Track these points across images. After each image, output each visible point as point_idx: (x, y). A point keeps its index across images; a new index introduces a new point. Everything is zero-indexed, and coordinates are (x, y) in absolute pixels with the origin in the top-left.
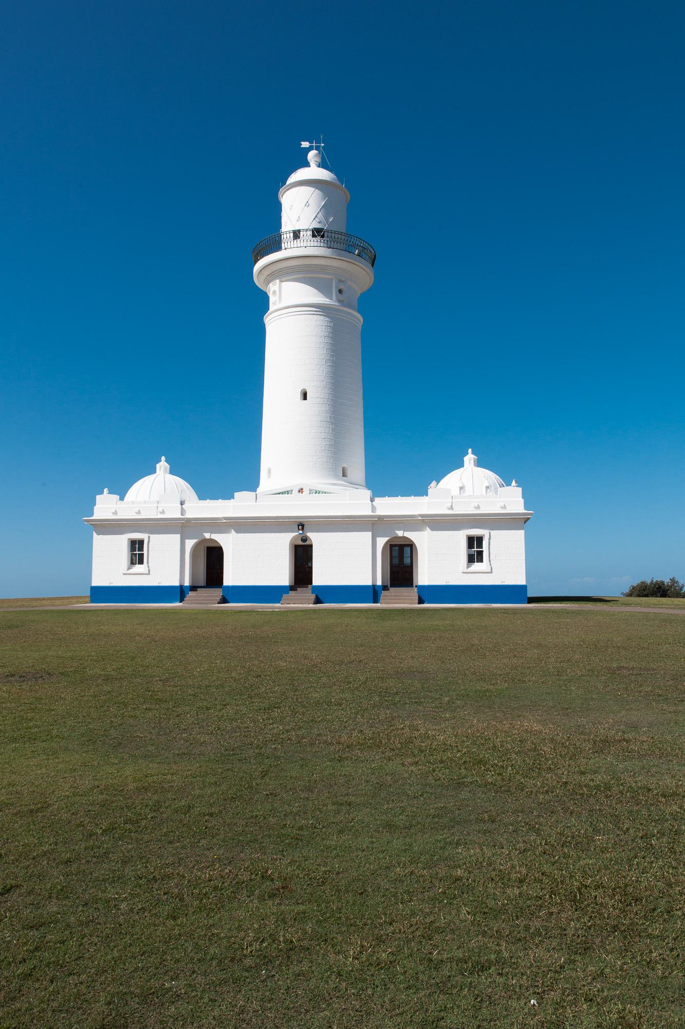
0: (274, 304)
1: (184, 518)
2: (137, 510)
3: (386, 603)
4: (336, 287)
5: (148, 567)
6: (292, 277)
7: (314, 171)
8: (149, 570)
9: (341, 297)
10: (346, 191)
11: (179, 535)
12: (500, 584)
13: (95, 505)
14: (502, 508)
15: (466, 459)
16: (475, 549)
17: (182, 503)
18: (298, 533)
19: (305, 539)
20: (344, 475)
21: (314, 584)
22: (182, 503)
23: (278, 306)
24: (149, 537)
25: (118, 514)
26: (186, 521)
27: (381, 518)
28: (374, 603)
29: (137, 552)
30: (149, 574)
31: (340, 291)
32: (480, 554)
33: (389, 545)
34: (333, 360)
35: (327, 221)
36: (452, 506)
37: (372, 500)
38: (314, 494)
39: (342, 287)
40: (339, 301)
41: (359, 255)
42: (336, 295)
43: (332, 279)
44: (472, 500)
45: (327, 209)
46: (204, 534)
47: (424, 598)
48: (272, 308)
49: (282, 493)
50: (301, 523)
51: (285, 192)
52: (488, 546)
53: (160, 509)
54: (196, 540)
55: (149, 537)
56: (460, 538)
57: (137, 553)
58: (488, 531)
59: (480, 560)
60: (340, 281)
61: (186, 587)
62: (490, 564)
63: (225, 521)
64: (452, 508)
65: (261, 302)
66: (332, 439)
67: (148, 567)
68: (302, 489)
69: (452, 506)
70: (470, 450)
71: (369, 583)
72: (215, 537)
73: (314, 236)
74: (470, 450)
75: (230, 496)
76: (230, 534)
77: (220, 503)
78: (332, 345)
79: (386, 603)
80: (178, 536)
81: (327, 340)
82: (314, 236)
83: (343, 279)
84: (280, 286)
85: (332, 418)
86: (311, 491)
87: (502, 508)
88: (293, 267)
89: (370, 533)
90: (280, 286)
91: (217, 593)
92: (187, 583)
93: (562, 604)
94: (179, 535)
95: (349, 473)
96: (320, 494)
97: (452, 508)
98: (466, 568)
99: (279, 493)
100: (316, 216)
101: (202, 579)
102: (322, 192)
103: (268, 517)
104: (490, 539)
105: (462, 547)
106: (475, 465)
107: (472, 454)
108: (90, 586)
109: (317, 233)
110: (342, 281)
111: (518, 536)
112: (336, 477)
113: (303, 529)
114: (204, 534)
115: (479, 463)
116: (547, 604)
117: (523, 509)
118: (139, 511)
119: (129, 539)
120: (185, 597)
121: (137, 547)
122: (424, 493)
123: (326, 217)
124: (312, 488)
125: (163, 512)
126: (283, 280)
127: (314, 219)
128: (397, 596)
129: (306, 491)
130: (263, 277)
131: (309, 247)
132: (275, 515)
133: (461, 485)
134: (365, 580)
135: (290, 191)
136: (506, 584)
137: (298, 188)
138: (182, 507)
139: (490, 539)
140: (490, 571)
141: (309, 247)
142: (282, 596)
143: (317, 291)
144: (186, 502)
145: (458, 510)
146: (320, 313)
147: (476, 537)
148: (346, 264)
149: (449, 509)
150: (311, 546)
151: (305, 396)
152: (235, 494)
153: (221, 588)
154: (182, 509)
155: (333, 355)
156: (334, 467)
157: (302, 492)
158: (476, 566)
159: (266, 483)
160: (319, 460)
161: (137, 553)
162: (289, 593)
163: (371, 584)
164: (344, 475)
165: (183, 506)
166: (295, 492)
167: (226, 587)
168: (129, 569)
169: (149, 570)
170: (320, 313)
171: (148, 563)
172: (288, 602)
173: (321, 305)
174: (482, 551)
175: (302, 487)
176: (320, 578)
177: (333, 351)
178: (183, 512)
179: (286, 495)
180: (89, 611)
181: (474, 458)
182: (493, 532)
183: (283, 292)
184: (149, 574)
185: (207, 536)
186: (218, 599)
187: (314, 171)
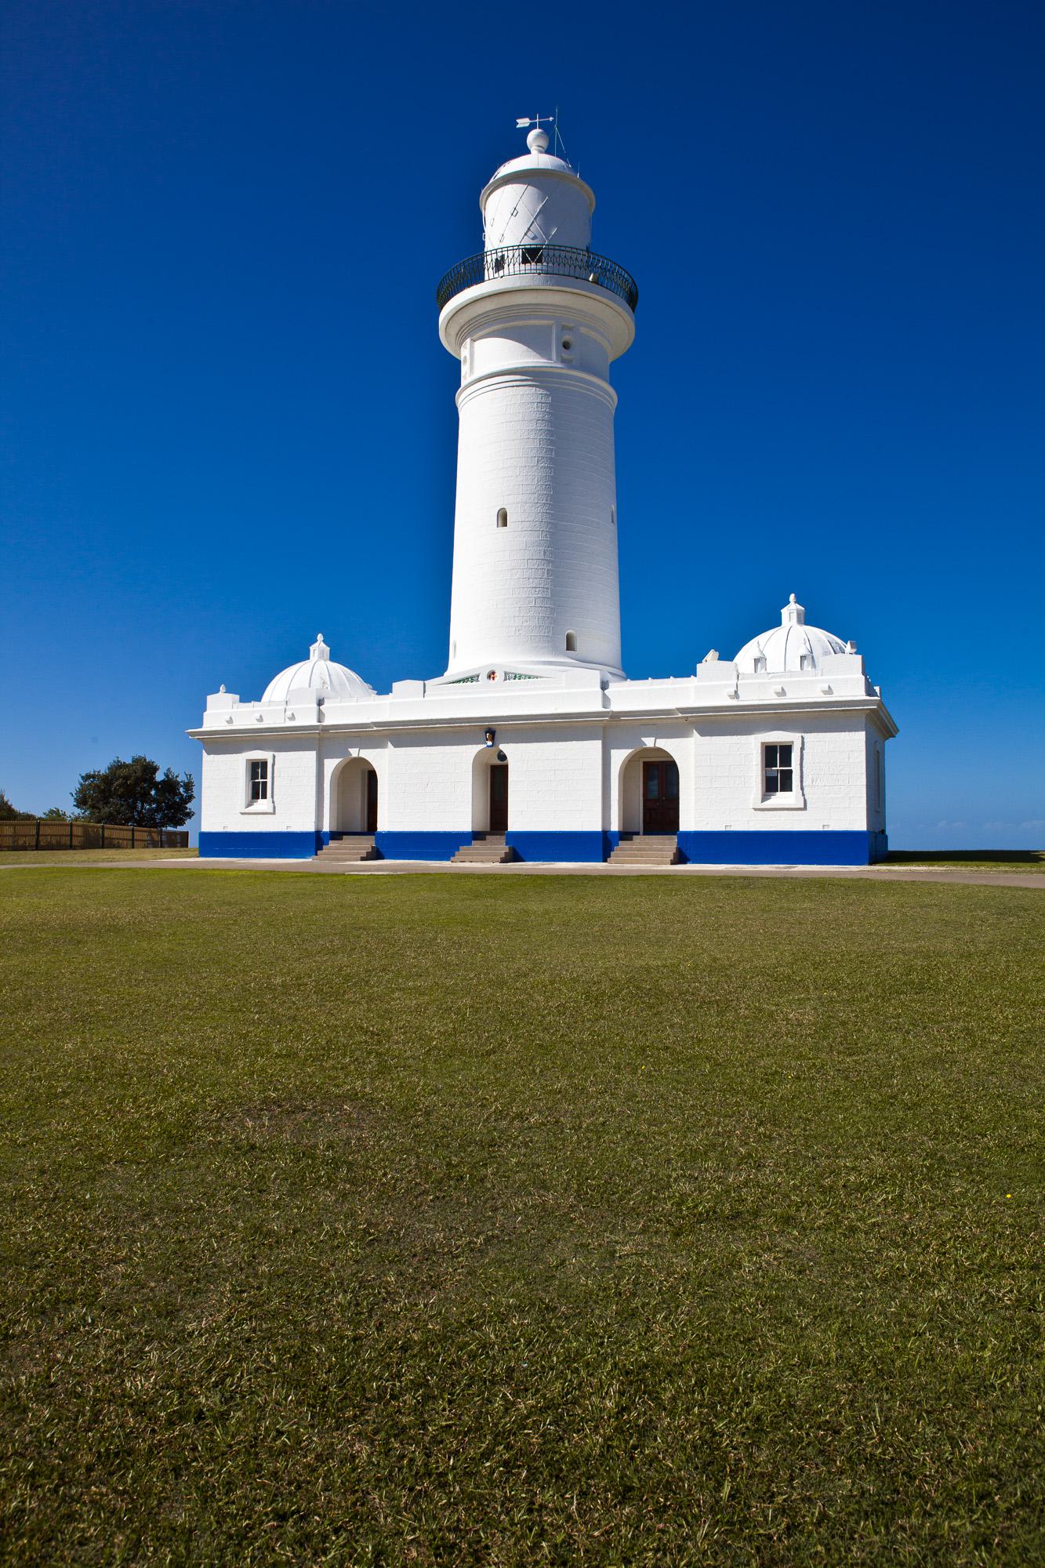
0: (465, 378)
1: (608, 712)
2: (257, 716)
3: (466, 863)
4: (558, 339)
5: (273, 802)
6: (481, 333)
7: (535, 159)
8: (274, 808)
9: (566, 354)
10: (584, 184)
11: (315, 752)
12: (723, 829)
13: (205, 710)
14: (825, 692)
15: (785, 612)
16: (778, 768)
17: (320, 703)
18: (485, 746)
19: (502, 757)
20: (570, 646)
21: (510, 829)
22: (320, 703)
23: (477, 374)
24: (274, 756)
25: (789, 695)
26: (611, 717)
27: (616, 716)
28: (871, 864)
29: (260, 780)
30: (805, 808)
31: (566, 346)
32: (787, 777)
33: (642, 765)
34: (551, 459)
35: (547, 234)
36: (736, 692)
37: (604, 686)
38: (512, 680)
39: (567, 337)
40: (563, 361)
41: (595, 281)
42: (557, 352)
43: (550, 327)
44: (773, 680)
45: (546, 216)
46: (643, 739)
47: (687, 853)
48: (464, 383)
49: (463, 680)
50: (490, 729)
51: (487, 199)
52: (799, 762)
53: (289, 714)
54: (630, 751)
55: (274, 756)
56: (749, 748)
57: (258, 783)
58: (800, 735)
59: (787, 786)
60: (564, 328)
61: (326, 833)
62: (803, 795)
63: (375, 728)
64: (736, 695)
65: (450, 372)
66: (547, 589)
67: (273, 802)
68: (493, 673)
69: (736, 692)
70: (792, 597)
71: (311, 828)
72: (664, 744)
73: (525, 261)
74: (792, 597)
75: (689, 671)
76: (689, 739)
77: (671, 683)
78: (550, 433)
79: (626, 862)
80: (314, 753)
81: (542, 426)
82: (525, 261)
83: (571, 325)
84: (472, 348)
85: (547, 554)
86: (507, 676)
87: (825, 692)
88: (485, 314)
89: (314, 753)
90: (472, 348)
91: (668, 845)
92: (615, 827)
93: (932, 866)
94: (315, 752)
95: (579, 643)
96: (522, 680)
97: (736, 695)
98: (760, 797)
99: (459, 681)
100: (529, 229)
101: (484, 825)
102: (538, 188)
103: (437, 720)
104: (802, 749)
105: (755, 763)
106: (799, 622)
107: (796, 602)
108: (198, 832)
109: (530, 255)
110: (570, 329)
111: (307, 759)
112: (555, 650)
113: (493, 739)
114: (643, 739)
115: (809, 618)
116: (919, 866)
117: (864, 693)
118: (231, 718)
119: (762, 743)
120: (612, 850)
121: (258, 770)
122: (690, 672)
123: (545, 229)
124: (508, 670)
125: (293, 718)
126: (475, 337)
127: (526, 234)
128: (644, 850)
129: (499, 676)
130: (454, 330)
131: (514, 277)
132: (505, 714)
133: (758, 655)
134: (589, 821)
135: (492, 196)
136: (830, 829)
137: (502, 189)
138: (320, 711)
139: (802, 749)
140: (272, 811)
141: (514, 277)
142: (458, 850)
143: (525, 348)
144: (326, 700)
145: (748, 698)
146: (530, 383)
147: (781, 746)
148: (569, 296)
149: (731, 697)
150: (506, 767)
151: (503, 518)
152: (394, 684)
153: (374, 834)
154: (604, 696)
155: (551, 450)
156: (550, 634)
157: (493, 678)
158: (780, 798)
159: (459, 663)
160: (525, 624)
161: (258, 783)
162: (470, 844)
163: (470, 830)
164: (570, 646)
165: (606, 691)
166: (483, 677)
167: (380, 833)
168: (249, 805)
169: (274, 808)
170: (530, 383)
171: (272, 797)
172: (463, 859)
173: (537, 369)
174: (791, 771)
175: (494, 669)
176: (518, 821)
177: (552, 442)
178: (320, 716)
179: (469, 683)
180: (620, 877)
181: (798, 610)
182: (809, 737)
183: (476, 356)
184: (805, 808)
185: (649, 742)
186: (670, 855)
187: (535, 159)
